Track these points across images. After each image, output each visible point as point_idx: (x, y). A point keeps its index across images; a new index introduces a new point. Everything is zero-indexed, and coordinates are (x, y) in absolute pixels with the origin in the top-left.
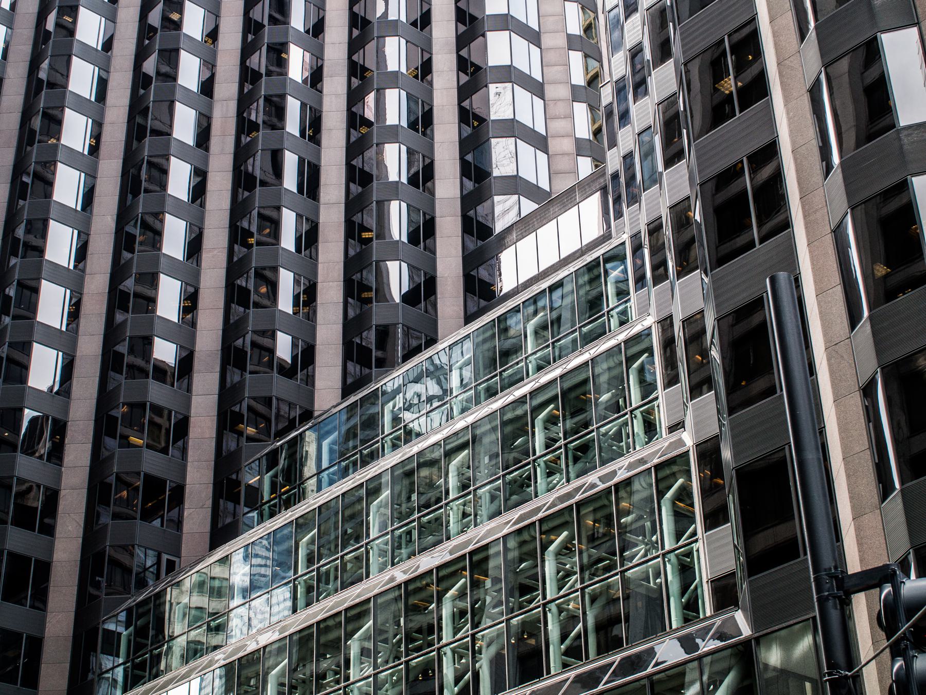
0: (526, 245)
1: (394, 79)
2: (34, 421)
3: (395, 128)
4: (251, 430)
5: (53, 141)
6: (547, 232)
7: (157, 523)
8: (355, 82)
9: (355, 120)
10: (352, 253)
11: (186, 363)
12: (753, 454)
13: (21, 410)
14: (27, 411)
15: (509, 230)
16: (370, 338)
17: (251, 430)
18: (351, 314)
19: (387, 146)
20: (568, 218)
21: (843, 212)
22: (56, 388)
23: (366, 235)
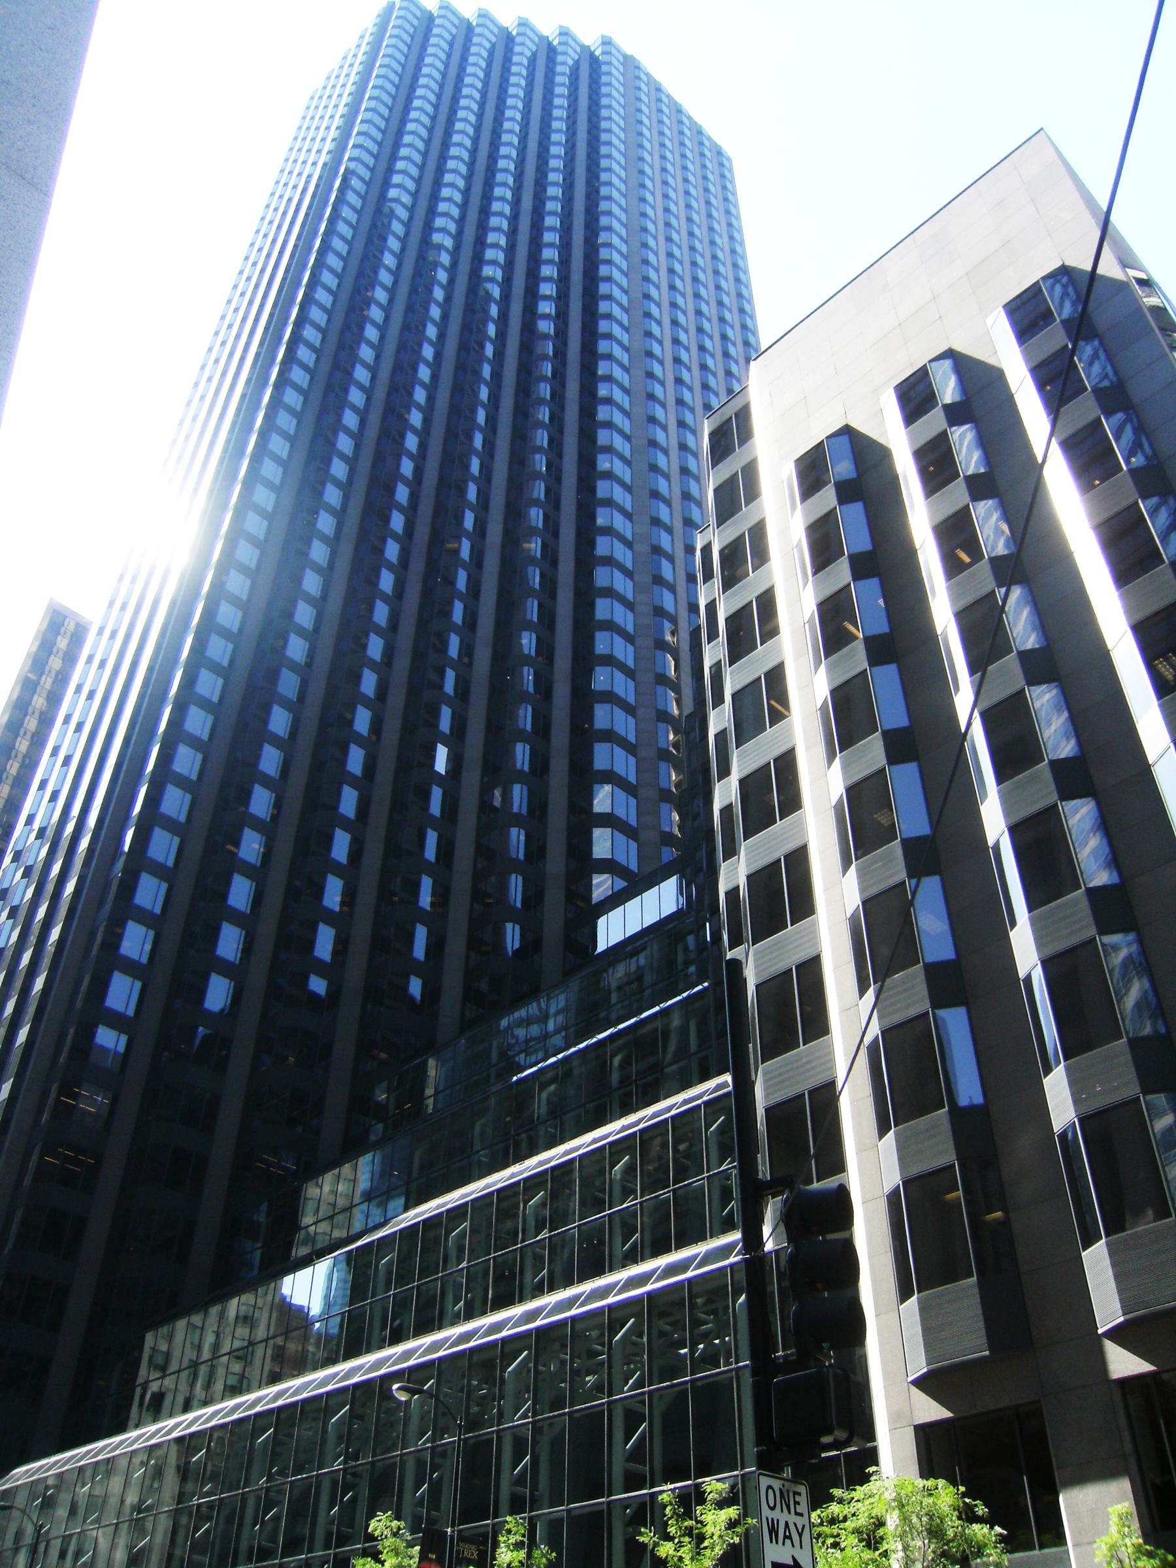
0: (616, 915)
1: (519, 777)
2: (206, 1038)
3: (518, 816)
4: (383, 1055)
5: (242, 809)
6: (633, 905)
7: (300, 1129)
8: (539, 175)
9: (485, 806)
10: (479, 866)
11: (334, 993)
12: (779, 1097)
13: (197, 1028)
14: (201, 1029)
15: (602, 903)
16: (484, 986)
17: (383, 1055)
18: (479, 866)
19: (512, 829)
20: (650, 895)
21: (1000, 832)
22: (226, 1011)
23: (484, 948)
